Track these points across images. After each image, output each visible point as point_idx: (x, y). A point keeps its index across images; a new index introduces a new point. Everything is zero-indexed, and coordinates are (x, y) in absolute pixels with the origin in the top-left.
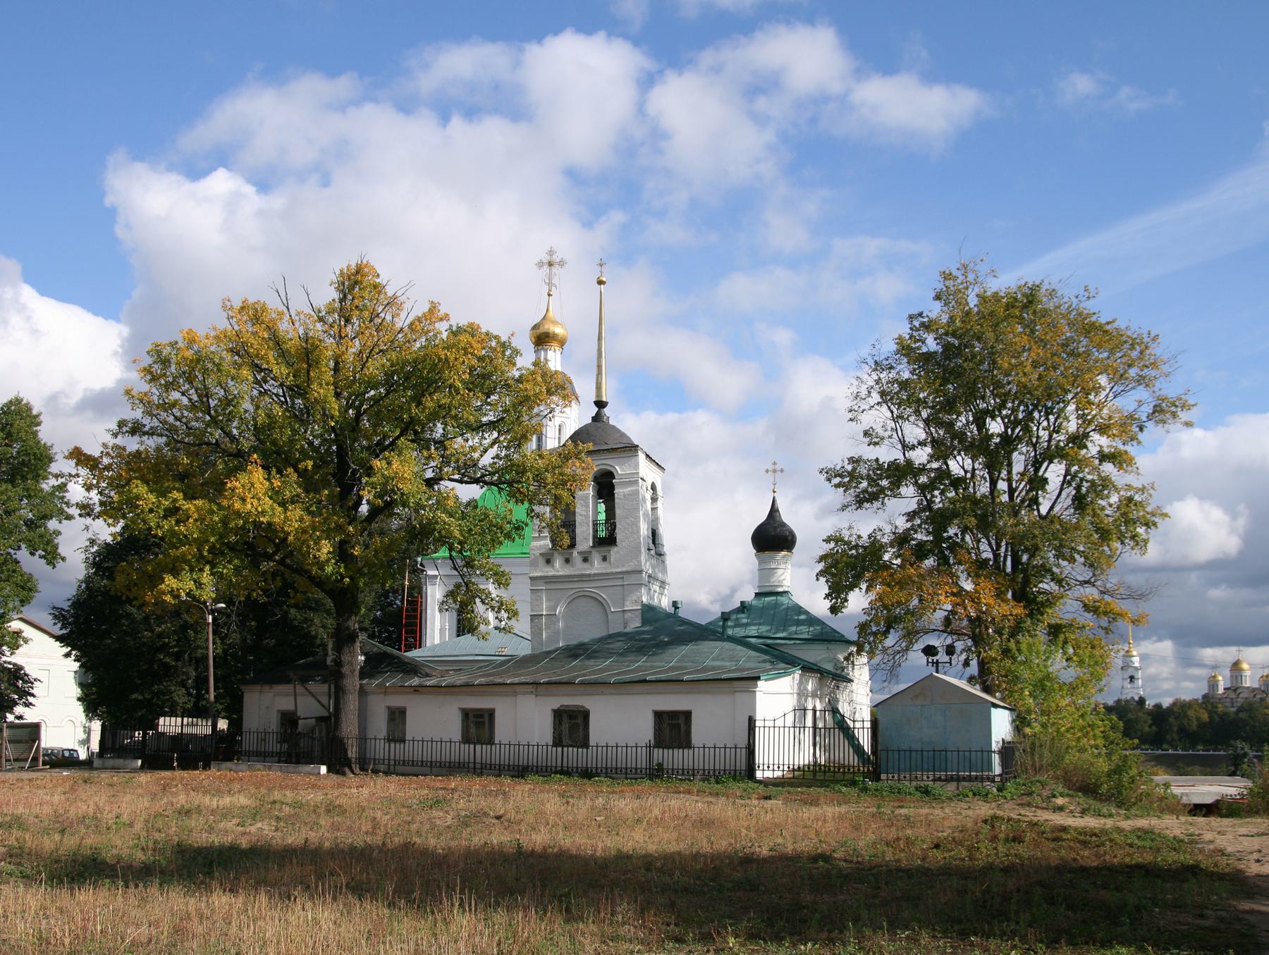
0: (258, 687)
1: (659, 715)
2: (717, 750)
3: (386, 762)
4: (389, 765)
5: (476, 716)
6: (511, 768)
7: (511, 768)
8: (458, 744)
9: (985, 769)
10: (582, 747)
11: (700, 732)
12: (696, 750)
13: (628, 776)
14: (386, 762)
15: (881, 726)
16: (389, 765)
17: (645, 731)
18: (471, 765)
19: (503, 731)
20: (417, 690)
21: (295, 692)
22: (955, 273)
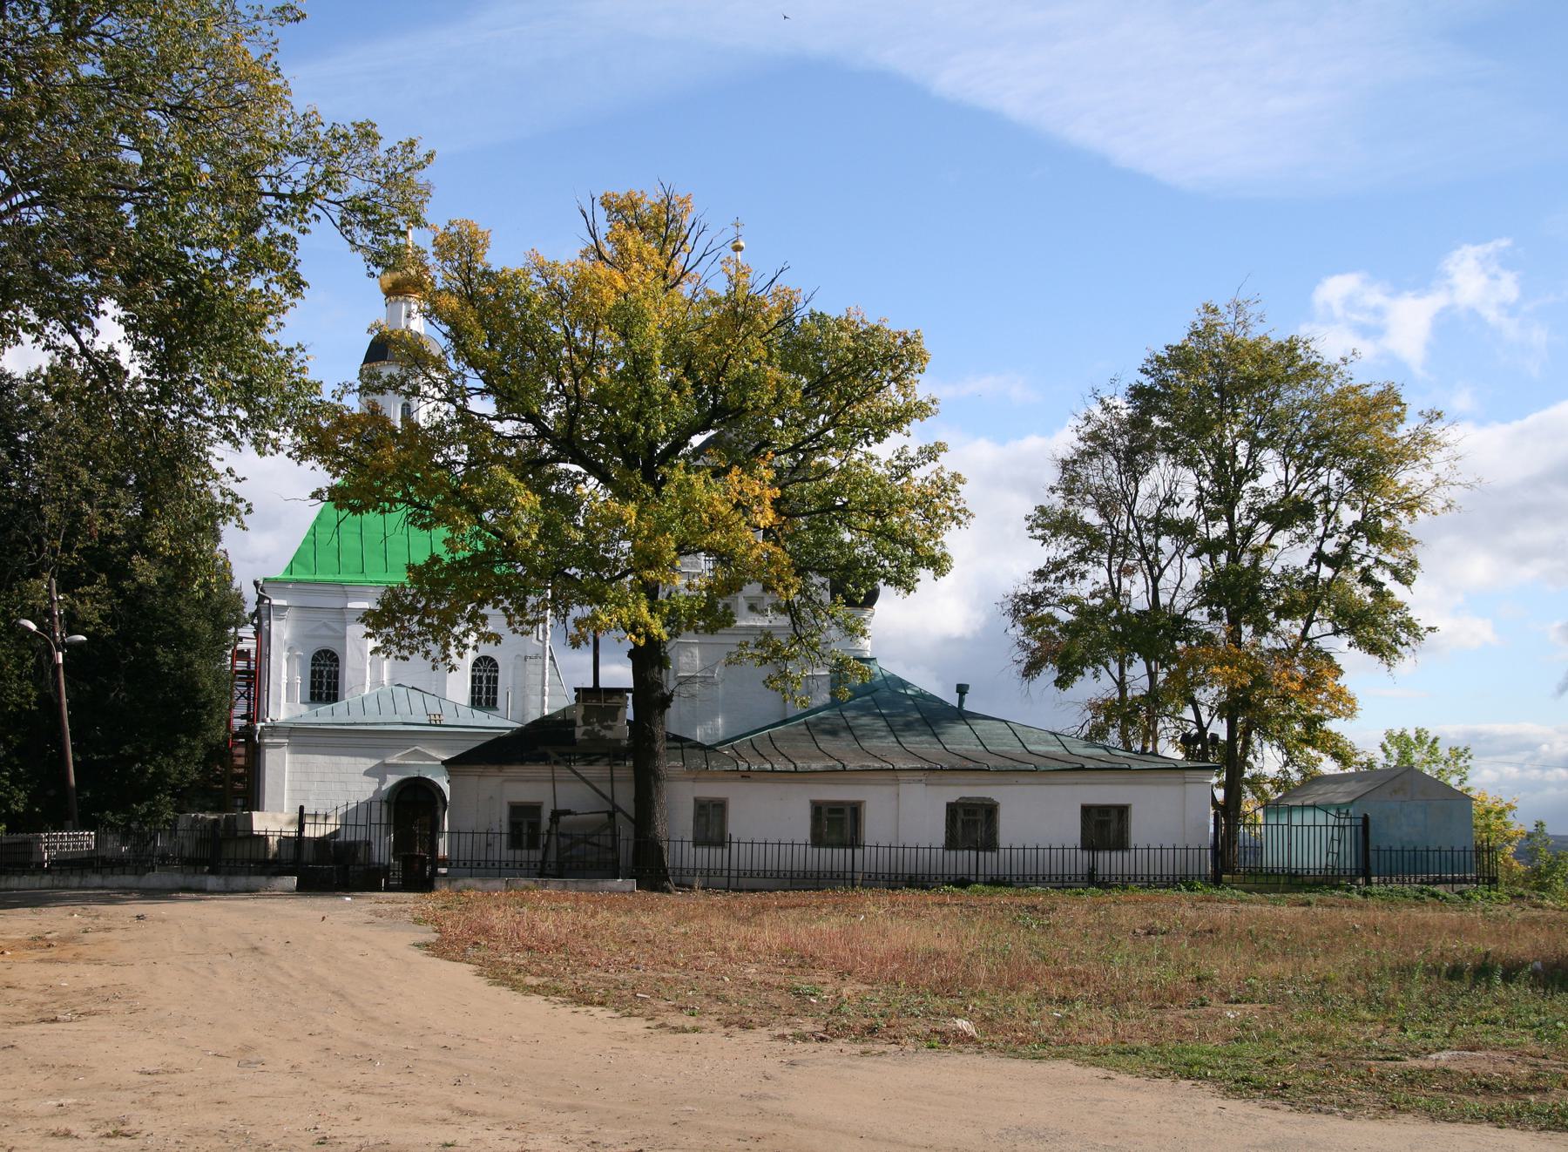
0: (478, 769)
1: (1086, 810)
2: (1152, 851)
4: (729, 877)
5: (831, 811)
10: (1117, 849)
11: (1141, 830)
12: (1001, 851)
14: (725, 873)
15: (1371, 825)
16: (729, 877)
17: (1070, 830)
18: (849, 875)
19: (875, 828)
20: (747, 775)
22: (1222, 310)
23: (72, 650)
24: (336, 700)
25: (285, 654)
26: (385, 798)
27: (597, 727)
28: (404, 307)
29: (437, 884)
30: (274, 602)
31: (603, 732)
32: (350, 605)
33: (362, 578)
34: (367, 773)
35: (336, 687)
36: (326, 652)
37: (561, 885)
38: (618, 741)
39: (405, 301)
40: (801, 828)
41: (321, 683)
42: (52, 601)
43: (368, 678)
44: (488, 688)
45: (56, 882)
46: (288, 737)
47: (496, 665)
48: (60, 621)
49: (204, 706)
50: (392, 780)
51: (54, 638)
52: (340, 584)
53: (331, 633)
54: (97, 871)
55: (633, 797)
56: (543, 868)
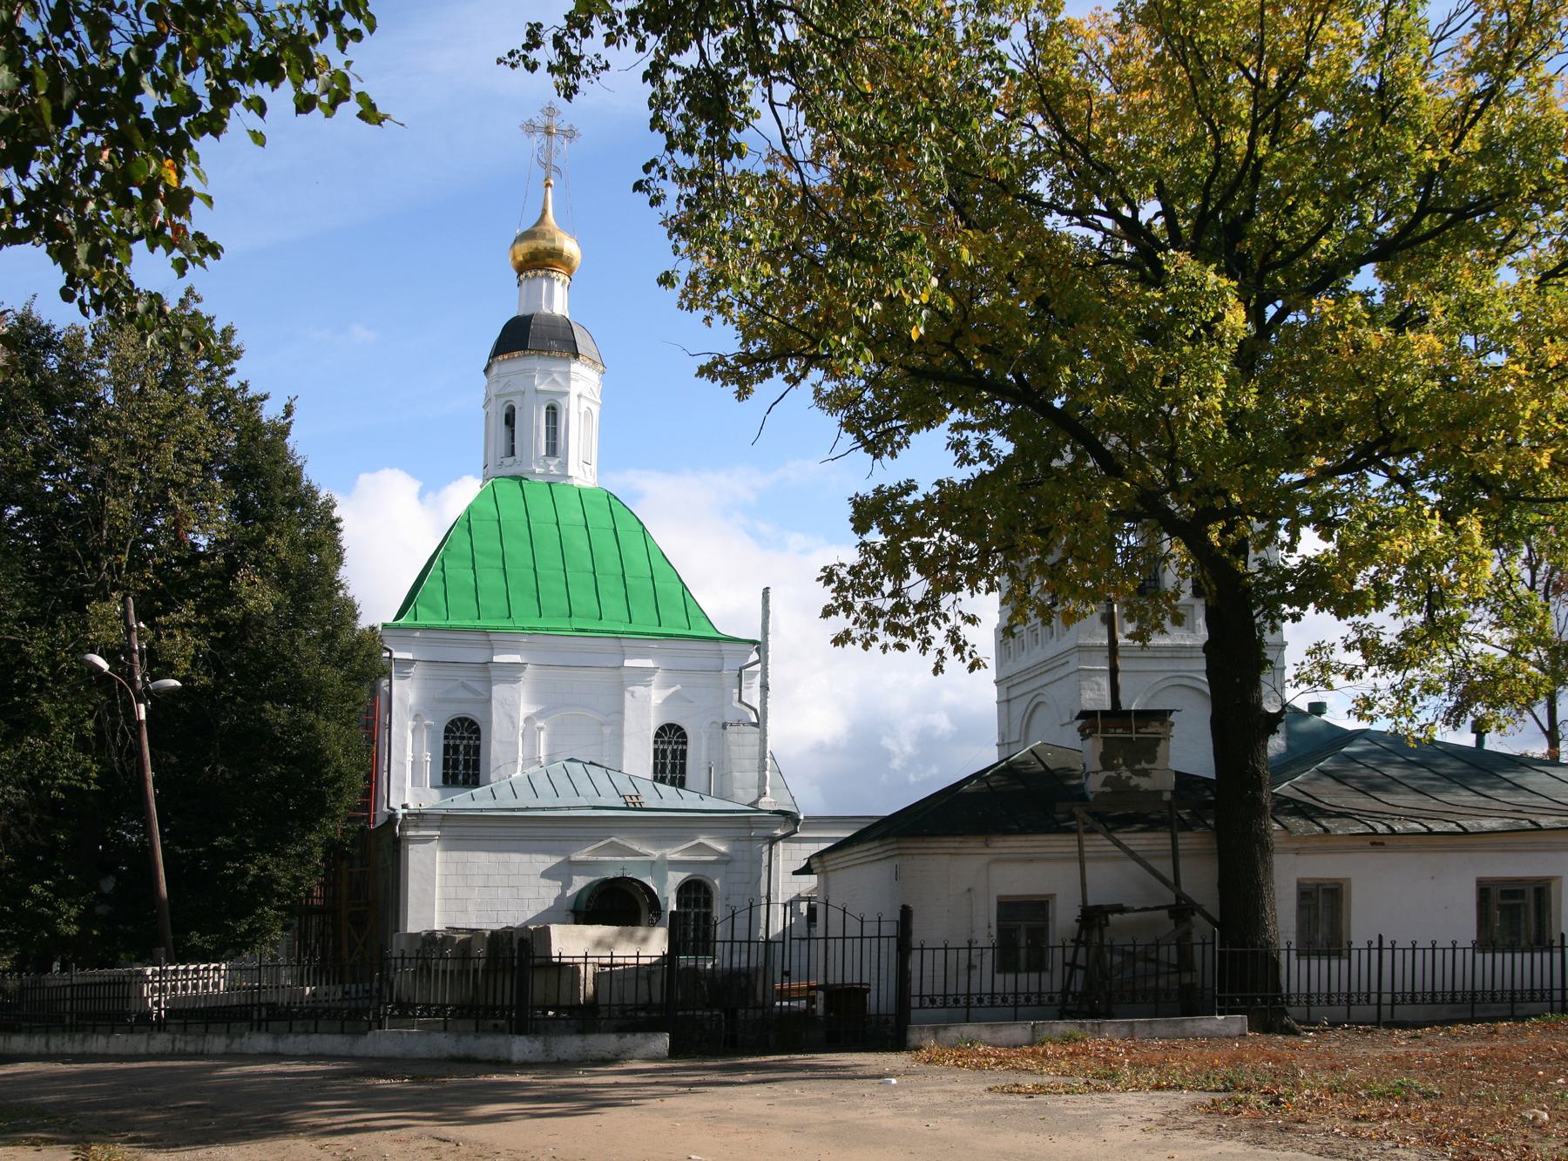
3: (1374, 998)
5: (1507, 894)
6: (1046, 998)
7: (1046, 998)
8: (1469, 953)
9: (607, 978)
10: (1329, 955)
13: (1020, 1010)
14: (1374, 998)
20: (1375, 842)
21: (1081, 851)
23: (161, 704)
24: (476, 784)
25: (410, 724)
26: (571, 906)
27: (1125, 774)
28: (545, 284)
29: (914, 1037)
30: (396, 655)
31: (1135, 781)
32: (496, 659)
33: (507, 623)
34: (546, 874)
35: (477, 765)
36: (462, 720)
37: (1125, 1030)
38: (1159, 793)
39: (547, 277)
40: (1463, 925)
41: (456, 762)
42: (129, 630)
43: (520, 754)
44: (674, 766)
45: (179, 1045)
46: (439, 828)
47: (684, 735)
48: (141, 658)
49: (330, 783)
50: (580, 883)
51: (132, 683)
52: (484, 631)
53: (471, 696)
54: (259, 1026)
55: (1217, 881)
56: (1064, 1001)
